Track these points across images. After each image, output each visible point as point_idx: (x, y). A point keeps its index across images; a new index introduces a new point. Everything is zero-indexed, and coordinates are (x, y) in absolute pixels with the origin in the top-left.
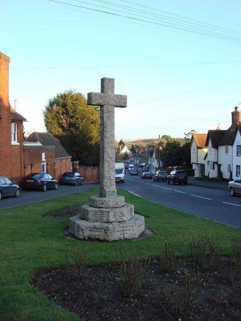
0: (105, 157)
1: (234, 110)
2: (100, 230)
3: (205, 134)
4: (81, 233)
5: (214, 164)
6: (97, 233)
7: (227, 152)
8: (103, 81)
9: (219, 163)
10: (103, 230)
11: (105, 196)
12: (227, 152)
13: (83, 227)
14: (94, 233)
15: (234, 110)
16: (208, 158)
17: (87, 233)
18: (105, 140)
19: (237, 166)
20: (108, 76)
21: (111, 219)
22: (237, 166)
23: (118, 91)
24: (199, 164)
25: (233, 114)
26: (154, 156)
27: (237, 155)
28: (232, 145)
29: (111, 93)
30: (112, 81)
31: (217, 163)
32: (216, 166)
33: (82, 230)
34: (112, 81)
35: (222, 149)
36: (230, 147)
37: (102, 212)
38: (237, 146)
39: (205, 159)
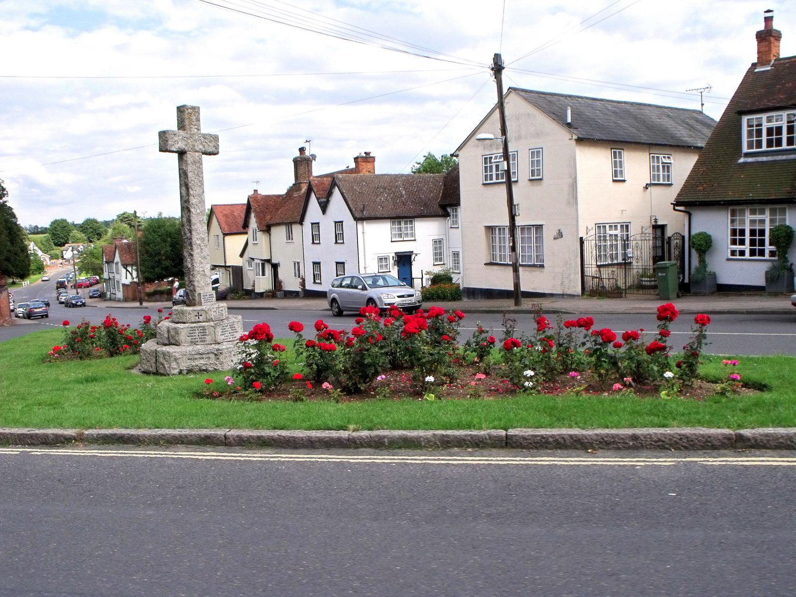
0: (194, 240)
1: (298, 154)
2: (207, 356)
3: (244, 204)
4: (174, 365)
5: (263, 265)
6: (202, 362)
7: (290, 236)
8: (181, 110)
9: (274, 261)
10: (212, 356)
11: (200, 304)
12: (290, 236)
13: (177, 355)
14: (197, 362)
15: (298, 154)
16: (249, 253)
17: (184, 365)
18: (192, 210)
19: (314, 263)
20: (189, 103)
21: (220, 338)
22: (314, 263)
23: (371, 155)
24: (229, 267)
25: (296, 162)
26: (117, 258)
27: (313, 243)
28: (301, 222)
29: (196, 130)
30: (196, 110)
31: (269, 261)
32: (268, 269)
33: (176, 360)
34: (196, 110)
35: (279, 233)
36: (296, 228)
37: (204, 328)
38: (336, 222)
39: (242, 255)
